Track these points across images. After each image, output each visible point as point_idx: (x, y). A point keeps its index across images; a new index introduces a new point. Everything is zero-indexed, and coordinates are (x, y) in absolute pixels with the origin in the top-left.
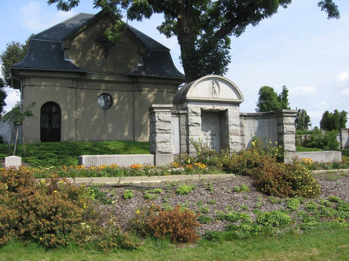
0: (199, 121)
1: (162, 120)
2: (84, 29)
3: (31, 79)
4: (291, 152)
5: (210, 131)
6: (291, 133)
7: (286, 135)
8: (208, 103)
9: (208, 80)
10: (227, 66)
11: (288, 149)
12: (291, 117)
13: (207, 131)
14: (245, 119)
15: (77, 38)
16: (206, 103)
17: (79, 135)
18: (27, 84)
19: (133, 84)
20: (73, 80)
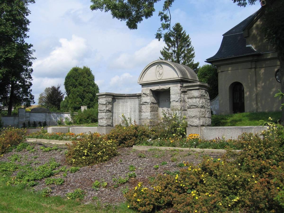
0: (147, 100)
3: (221, 66)
4: (194, 127)
6: (195, 107)
8: (155, 85)
9: (154, 65)
15: (254, 26)
17: (261, 107)
18: (220, 71)
20: (252, 61)
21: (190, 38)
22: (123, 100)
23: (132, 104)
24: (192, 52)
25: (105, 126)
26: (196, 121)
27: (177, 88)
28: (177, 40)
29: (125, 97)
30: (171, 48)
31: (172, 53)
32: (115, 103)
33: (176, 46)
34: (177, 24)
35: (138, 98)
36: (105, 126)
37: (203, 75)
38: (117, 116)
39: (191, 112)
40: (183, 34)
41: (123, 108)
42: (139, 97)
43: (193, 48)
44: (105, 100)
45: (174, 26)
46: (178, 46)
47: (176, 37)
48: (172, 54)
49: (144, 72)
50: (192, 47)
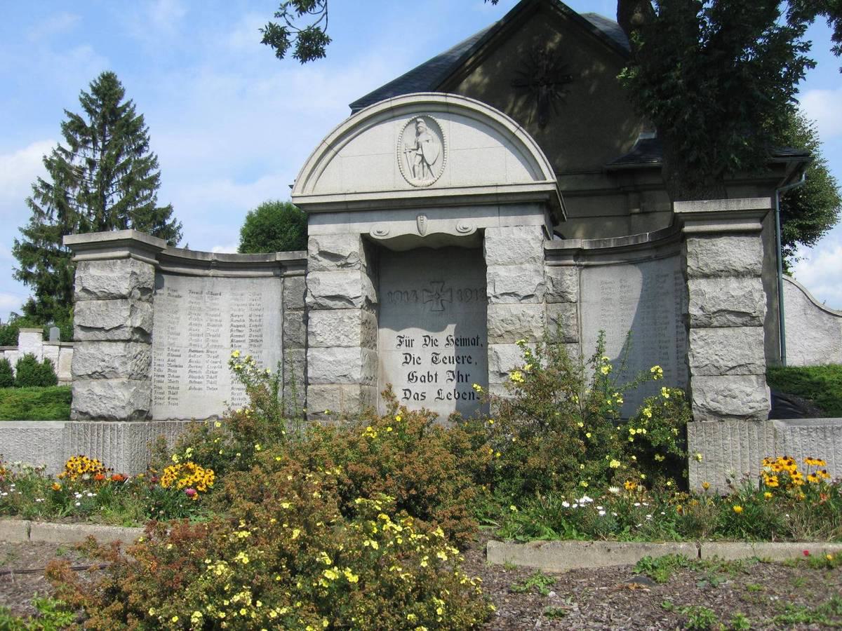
1: (95, 293)
2: (480, 56)
4: (734, 421)
5: (454, 326)
6: (739, 320)
7: (702, 332)
9: (394, 118)
10: (800, 80)
11: (713, 405)
12: (734, 240)
13: (441, 328)
14: (587, 266)
16: (386, 212)
19: (626, 193)
21: (148, 128)
22: (195, 284)
23: (240, 303)
24: (152, 173)
25: (124, 419)
26: (749, 390)
27: (527, 232)
28: (102, 126)
29: (207, 265)
30: (81, 151)
31: (84, 169)
32: (158, 296)
33: (100, 144)
34: (107, 73)
35: (276, 276)
36: (121, 420)
37: (262, 238)
38: (165, 363)
39: (718, 347)
40: (125, 111)
41: (194, 322)
42: (289, 272)
43: (155, 159)
44: (129, 270)
45: (95, 81)
46: (103, 145)
47: (104, 116)
48: (81, 170)
49: (330, 148)
50: (151, 155)
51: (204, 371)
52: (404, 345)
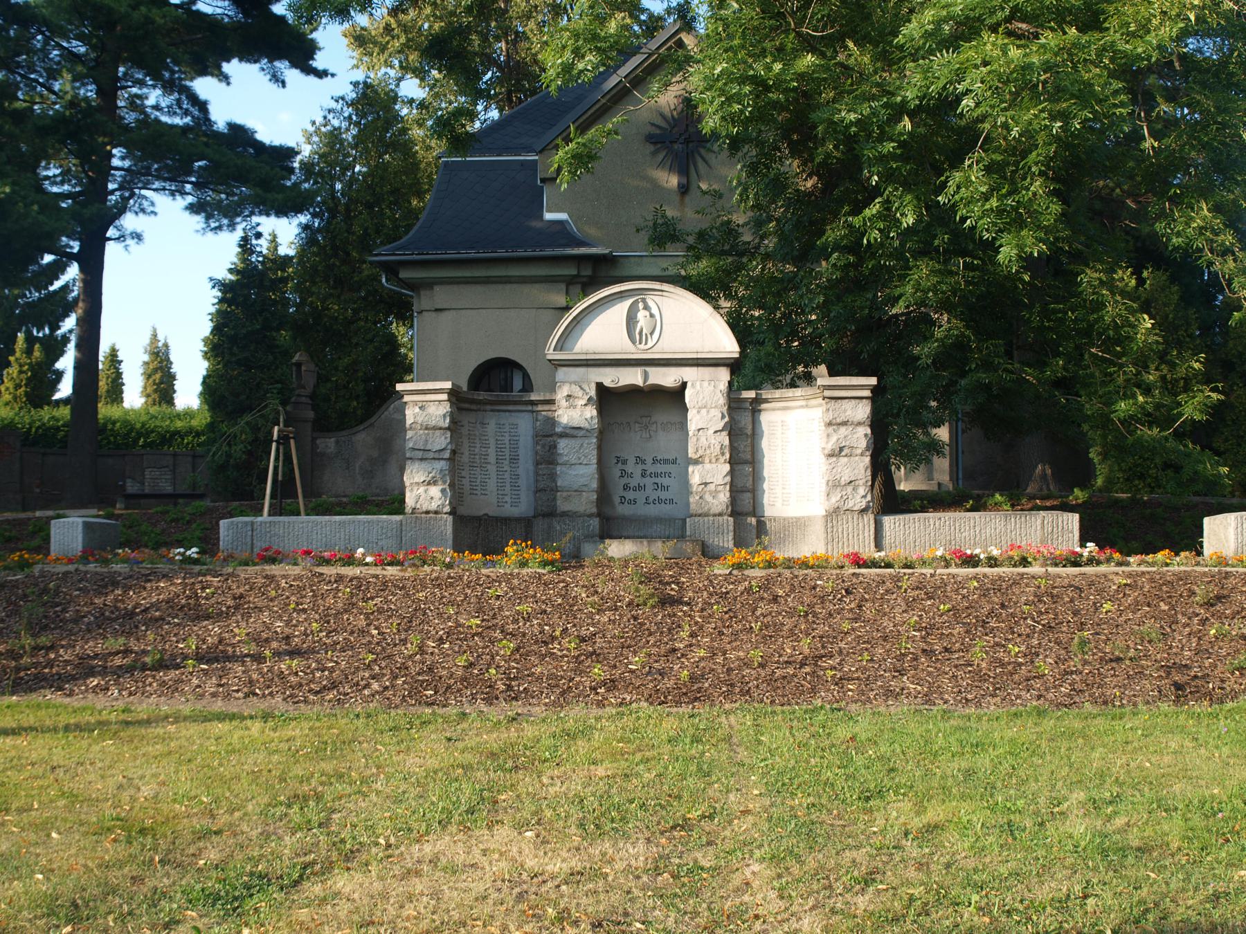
51: (479, 481)
52: (620, 464)
